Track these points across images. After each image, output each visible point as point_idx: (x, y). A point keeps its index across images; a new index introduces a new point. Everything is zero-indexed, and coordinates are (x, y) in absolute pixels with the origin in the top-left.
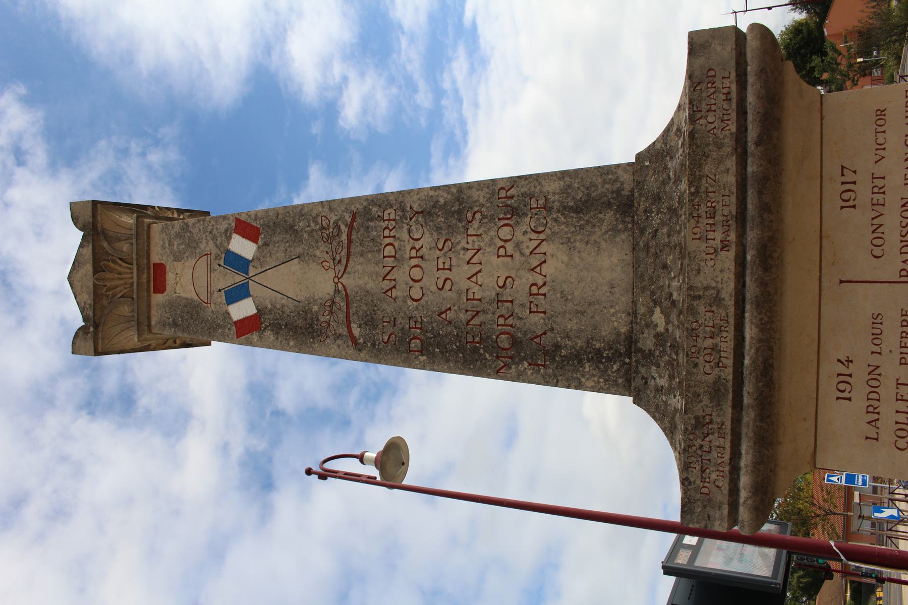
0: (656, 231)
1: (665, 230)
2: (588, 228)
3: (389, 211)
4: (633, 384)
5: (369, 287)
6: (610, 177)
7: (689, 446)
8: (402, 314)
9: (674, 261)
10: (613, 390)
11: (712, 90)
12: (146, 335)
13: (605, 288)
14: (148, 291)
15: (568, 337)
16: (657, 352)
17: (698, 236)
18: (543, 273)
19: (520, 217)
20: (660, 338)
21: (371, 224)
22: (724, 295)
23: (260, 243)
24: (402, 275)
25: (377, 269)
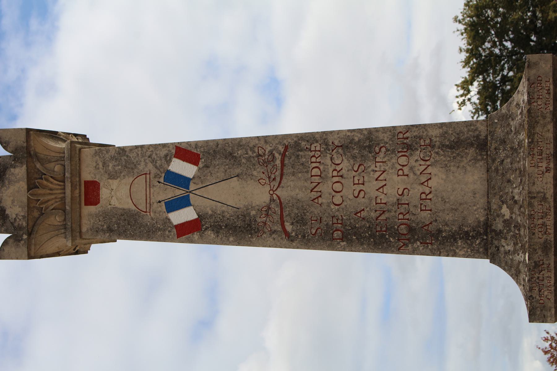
0: (503, 161)
1: (509, 160)
2: (459, 158)
3: (315, 145)
4: (490, 251)
5: (299, 197)
6: (472, 127)
7: (532, 278)
8: (326, 214)
9: (515, 178)
10: (477, 256)
11: (540, 88)
12: (78, 241)
13: (470, 194)
14: (80, 204)
15: (447, 225)
16: (505, 231)
17: (533, 165)
18: (429, 186)
19: (413, 151)
20: (507, 223)
21: (301, 153)
22: (548, 196)
23: (201, 165)
24: (326, 188)
25: (306, 184)
